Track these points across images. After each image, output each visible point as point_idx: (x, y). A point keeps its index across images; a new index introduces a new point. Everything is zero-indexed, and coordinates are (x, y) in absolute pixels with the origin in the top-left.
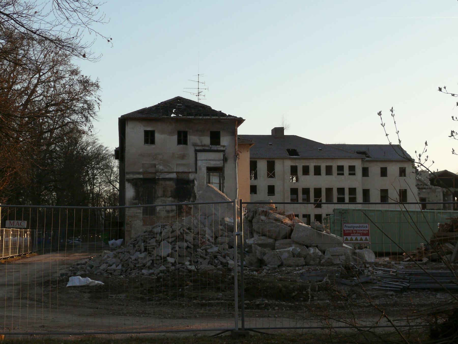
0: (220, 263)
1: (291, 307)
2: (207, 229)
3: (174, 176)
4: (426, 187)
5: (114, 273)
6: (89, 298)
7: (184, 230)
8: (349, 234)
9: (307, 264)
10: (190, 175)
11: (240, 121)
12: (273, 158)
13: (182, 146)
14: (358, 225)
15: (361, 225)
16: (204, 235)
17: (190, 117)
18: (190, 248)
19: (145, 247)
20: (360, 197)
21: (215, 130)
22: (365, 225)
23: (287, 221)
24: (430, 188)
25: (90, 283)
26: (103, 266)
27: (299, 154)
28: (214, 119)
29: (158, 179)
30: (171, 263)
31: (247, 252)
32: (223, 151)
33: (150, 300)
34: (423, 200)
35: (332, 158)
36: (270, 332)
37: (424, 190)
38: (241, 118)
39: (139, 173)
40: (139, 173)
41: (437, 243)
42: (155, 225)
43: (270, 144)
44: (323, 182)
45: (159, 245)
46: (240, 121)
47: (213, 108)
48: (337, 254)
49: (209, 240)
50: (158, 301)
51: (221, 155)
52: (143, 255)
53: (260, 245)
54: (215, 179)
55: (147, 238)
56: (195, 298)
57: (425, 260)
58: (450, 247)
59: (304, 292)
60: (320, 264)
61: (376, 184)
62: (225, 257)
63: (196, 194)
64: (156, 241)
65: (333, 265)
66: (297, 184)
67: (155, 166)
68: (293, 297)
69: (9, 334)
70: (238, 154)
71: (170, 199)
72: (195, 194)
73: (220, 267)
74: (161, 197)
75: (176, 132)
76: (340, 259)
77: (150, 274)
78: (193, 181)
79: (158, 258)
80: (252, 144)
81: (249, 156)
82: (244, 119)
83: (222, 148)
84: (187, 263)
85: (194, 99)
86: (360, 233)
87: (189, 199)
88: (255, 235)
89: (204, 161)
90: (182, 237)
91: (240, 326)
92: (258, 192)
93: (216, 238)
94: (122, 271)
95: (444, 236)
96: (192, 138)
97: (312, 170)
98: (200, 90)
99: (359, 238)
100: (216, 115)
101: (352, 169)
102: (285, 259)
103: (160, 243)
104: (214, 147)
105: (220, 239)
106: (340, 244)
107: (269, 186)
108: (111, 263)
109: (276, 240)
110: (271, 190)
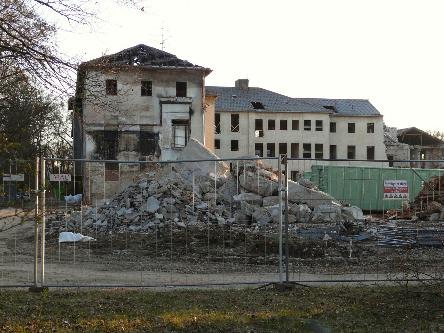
0: (209, 219)
1: (304, 262)
2: (193, 184)
3: (137, 128)
4: (394, 144)
5: (100, 229)
6: (91, 254)
8: (389, 191)
9: (298, 221)
10: (154, 128)
11: (207, 72)
12: (237, 112)
14: (398, 182)
15: (400, 182)
16: (192, 191)
17: (155, 66)
19: (131, 202)
20: (326, 154)
21: (181, 80)
22: (404, 182)
23: (275, 177)
24: (398, 146)
25: (83, 239)
27: (265, 107)
28: (180, 69)
29: (121, 131)
30: (160, 219)
31: (234, 208)
32: (190, 103)
33: (158, 255)
34: (390, 157)
35: (299, 113)
36: (311, 284)
37: (392, 147)
38: (208, 69)
39: (100, 125)
40: (100, 125)
41: (422, 201)
44: (289, 137)
45: (147, 201)
46: (207, 72)
47: (179, 57)
48: (328, 211)
49: (196, 196)
50: (167, 256)
51: (186, 108)
52: (130, 211)
53: (249, 202)
55: (133, 193)
56: (206, 254)
57: (414, 218)
58: (438, 206)
59: (314, 249)
60: (310, 221)
61: (343, 140)
62: (213, 214)
64: (143, 196)
65: (324, 222)
67: (117, 117)
68: (304, 253)
69: (57, 286)
70: (205, 107)
71: (134, 153)
72: (159, 148)
73: (210, 223)
74: (124, 150)
75: (175, 84)
76: (330, 217)
78: (157, 135)
79: (145, 214)
80: (217, 96)
82: (211, 69)
83: (188, 100)
84: (176, 219)
86: (400, 190)
87: (153, 153)
88: (242, 191)
89: (169, 114)
91: (284, 280)
92: (220, 147)
93: (203, 194)
94: (108, 226)
95: (429, 195)
96: (157, 89)
97: (277, 125)
99: (398, 195)
101: (319, 124)
102: (275, 216)
103: (147, 198)
104: (180, 99)
105: (208, 195)
106: (329, 201)
108: (96, 219)
109: (263, 196)
110: (235, 145)
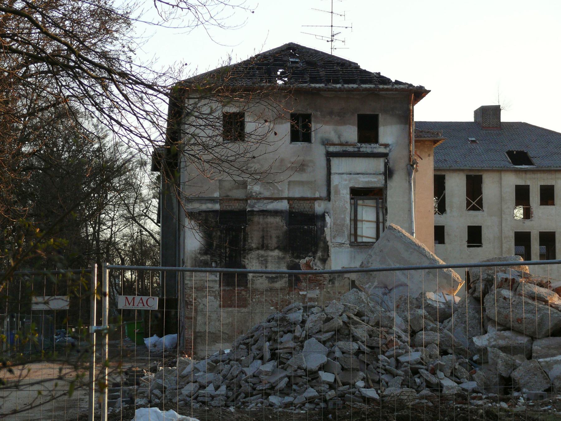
0: (424, 384)
2: (394, 314)
3: (284, 205)
7: (349, 318)
11: (420, 93)
12: (478, 170)
13: (299, 145)
17: (317, 85)
18: (363, 353)
19: (271, 350)
21: (367, 111)
26: (190, 388)
27: (534, 160)
28: (366, 89)
29: (252, 212)
30: (328, 383)
31: (475, 362)
32: (385, 155)
38: (421, 88)
39: (213, 200)
40: (213, 200)
42: (290, 306)
43: (472, 141)
45: (302, 347)
46: (420, 93)
47: (363, 67)
49: (399, 337)
51: (379, 165)
52: (269, 367)
53: (504, 349)
54: (367, 213)
62: (433, 372)
63: (329, 244)
64: (295, 338)
66: (527, 222)
67: (244, 185)
71: (276, 253)
72: (326, 242)
73: (426, 392)
74: (258, 249)
77: (287, 405)
79: (300, 372)
80: (438, 141)
81: (432, 167)
82: (427, 88)
83: (382, 150)
84: (360, 384)
85: (324, 47)
87: (315, 253)
88: (490, 328)
89: (345, 176)
90: (347, 332)
92: (446, 240)
94: (228, 397)
96: (322, 130)
98: (335, 30)
100: (370, 82)
103: (302, 342)
104: (366, 148)
105: (423, 336)
107: (469, 227)
108: (204, 382)
109: (533, 338)
110: (475, 236)
